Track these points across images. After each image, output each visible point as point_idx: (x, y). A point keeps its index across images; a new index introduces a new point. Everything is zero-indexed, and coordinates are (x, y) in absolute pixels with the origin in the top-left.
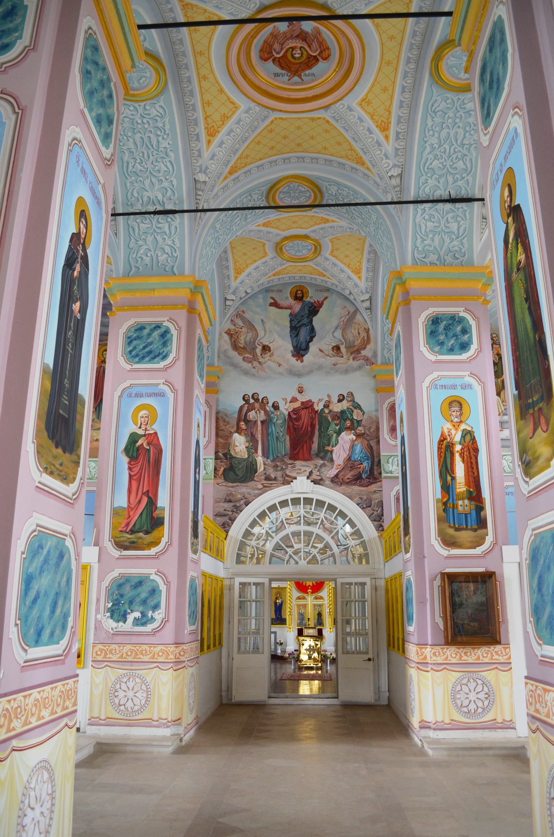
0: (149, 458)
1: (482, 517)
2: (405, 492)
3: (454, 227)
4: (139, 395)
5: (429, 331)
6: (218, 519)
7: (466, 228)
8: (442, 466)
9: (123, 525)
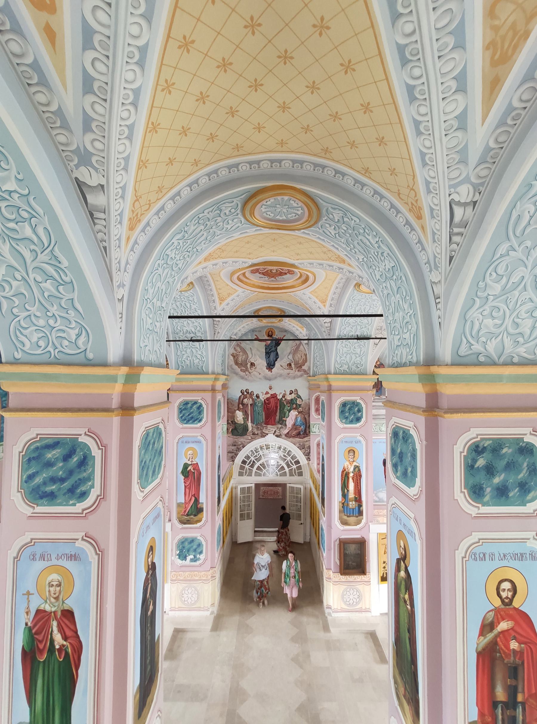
3: (358, 350)
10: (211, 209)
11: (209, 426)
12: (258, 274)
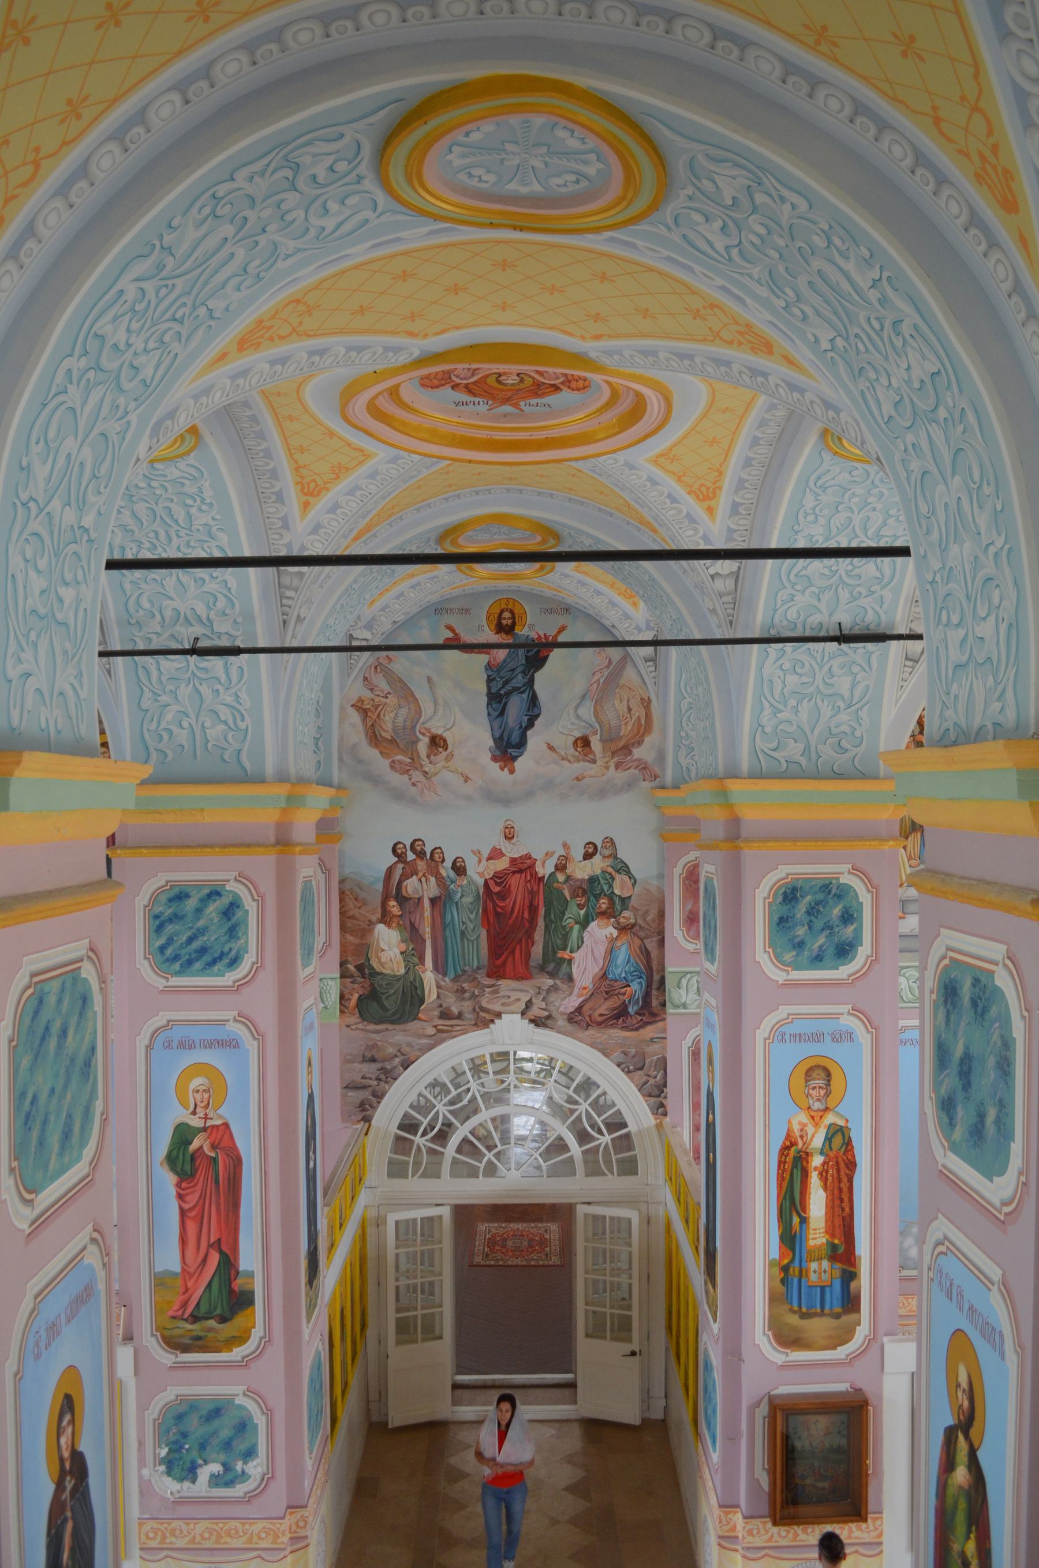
0: (217, 1176)
1: (852, 1291)
2: (711, 1201)
3: (843, 684)
4: (187, 1045)
5: (776, 919)
6: (350, 1094)
7: (868, 686)
8: (785, 1198)
9: (176, 1306)
10: (258, 166)
11: (267, 983)
12: (447, 391)
